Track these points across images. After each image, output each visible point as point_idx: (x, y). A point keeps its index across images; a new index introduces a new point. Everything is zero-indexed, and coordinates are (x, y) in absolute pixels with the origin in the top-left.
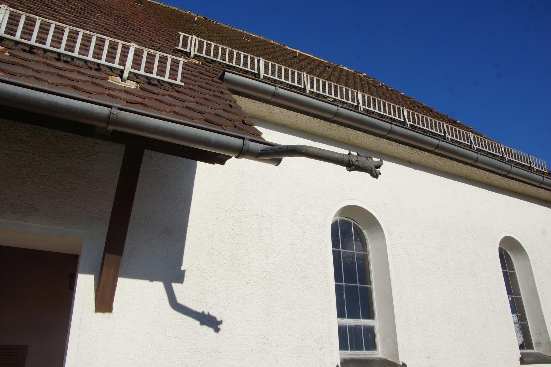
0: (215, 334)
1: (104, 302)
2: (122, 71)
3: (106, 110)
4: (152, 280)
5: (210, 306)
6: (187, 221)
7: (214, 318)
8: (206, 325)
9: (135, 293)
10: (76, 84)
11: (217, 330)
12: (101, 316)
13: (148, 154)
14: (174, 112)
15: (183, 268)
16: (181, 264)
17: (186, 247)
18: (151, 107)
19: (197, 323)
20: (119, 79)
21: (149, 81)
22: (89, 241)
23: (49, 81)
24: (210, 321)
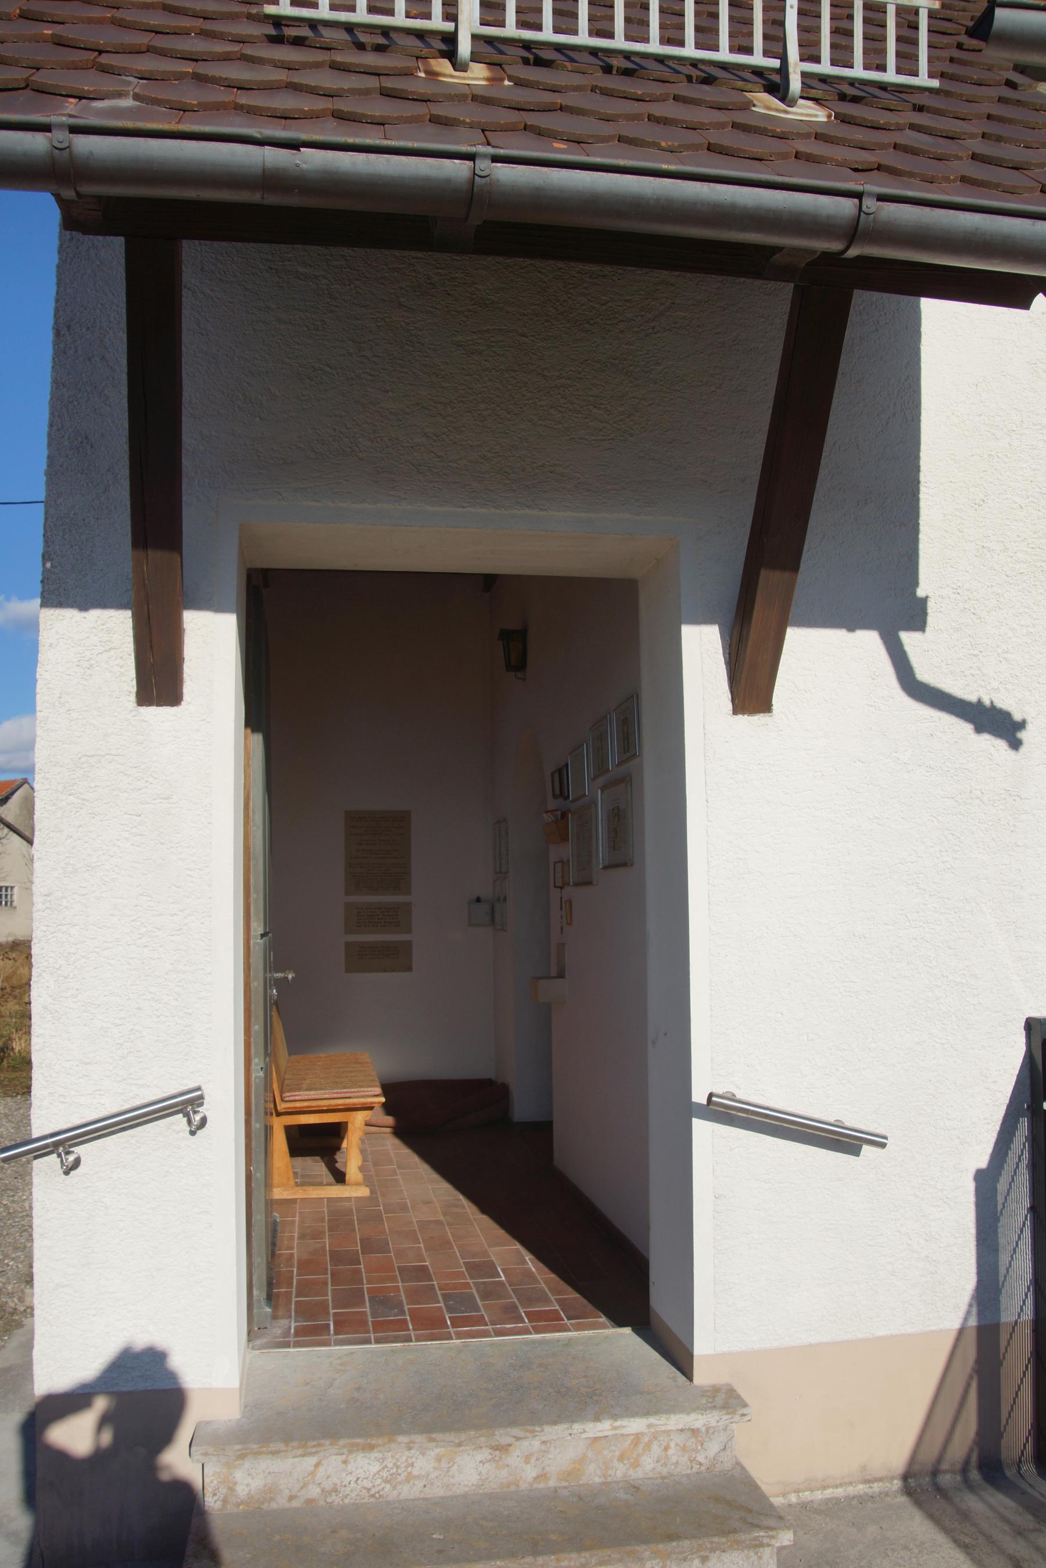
0: (1011, 753)
1: (751, 686)
2: (450, 39)
3: (846, 207)
4: (851, 629)
5: (995, 684)
6: (917, 469)
7: (1007, 715)
8: (989, 733)
9: (823, 661)
10: (341, 105)
11: (1015, 744)
12: (744, 720)
13: (863, 301)
14: (710, 148)
15: (920, 593)
16: (915, 583)
17: (922, 536)
18: (911, 175)
19: (968, 728)
20: (444, 66)
21: (535, 55)
22: (711, 541)
23: (663, 144)
24: (998, 724)
